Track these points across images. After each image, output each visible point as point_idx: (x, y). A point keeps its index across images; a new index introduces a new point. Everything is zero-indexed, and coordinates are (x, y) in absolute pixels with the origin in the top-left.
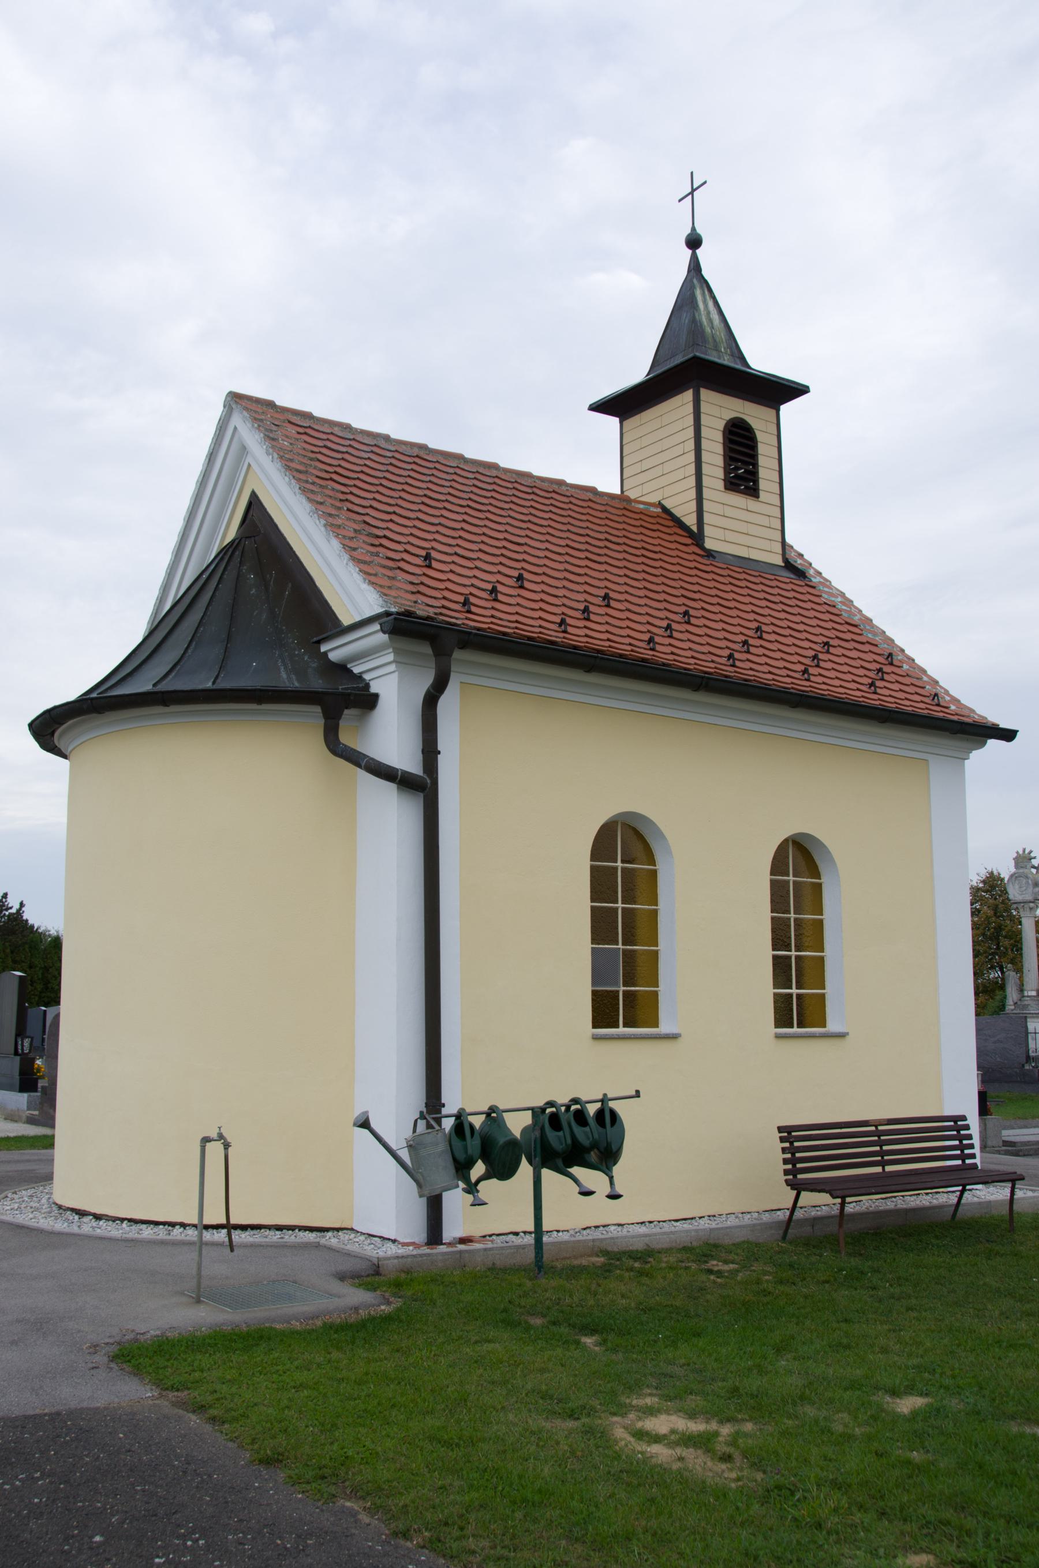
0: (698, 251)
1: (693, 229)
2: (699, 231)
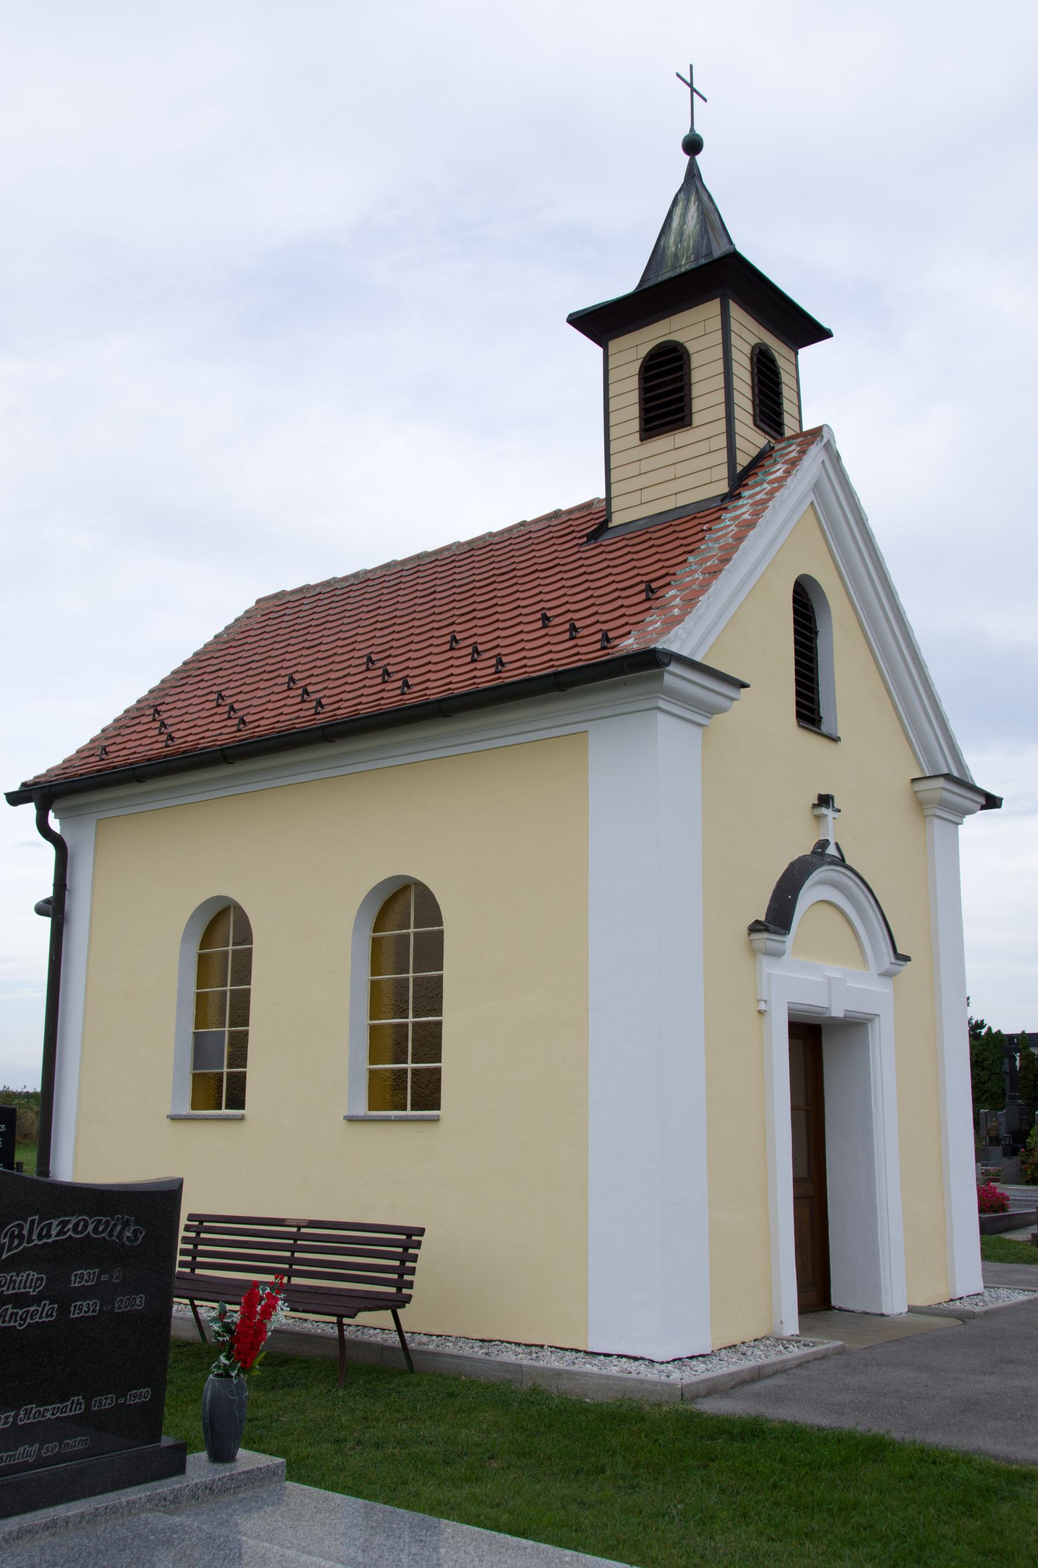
0: (697, 157)
1: (692, 129)
2: (698, 130)
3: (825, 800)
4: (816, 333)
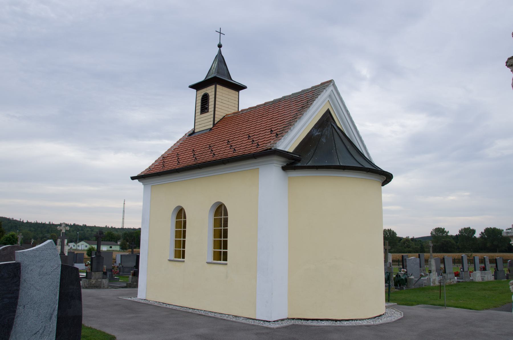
2: (221, 43)
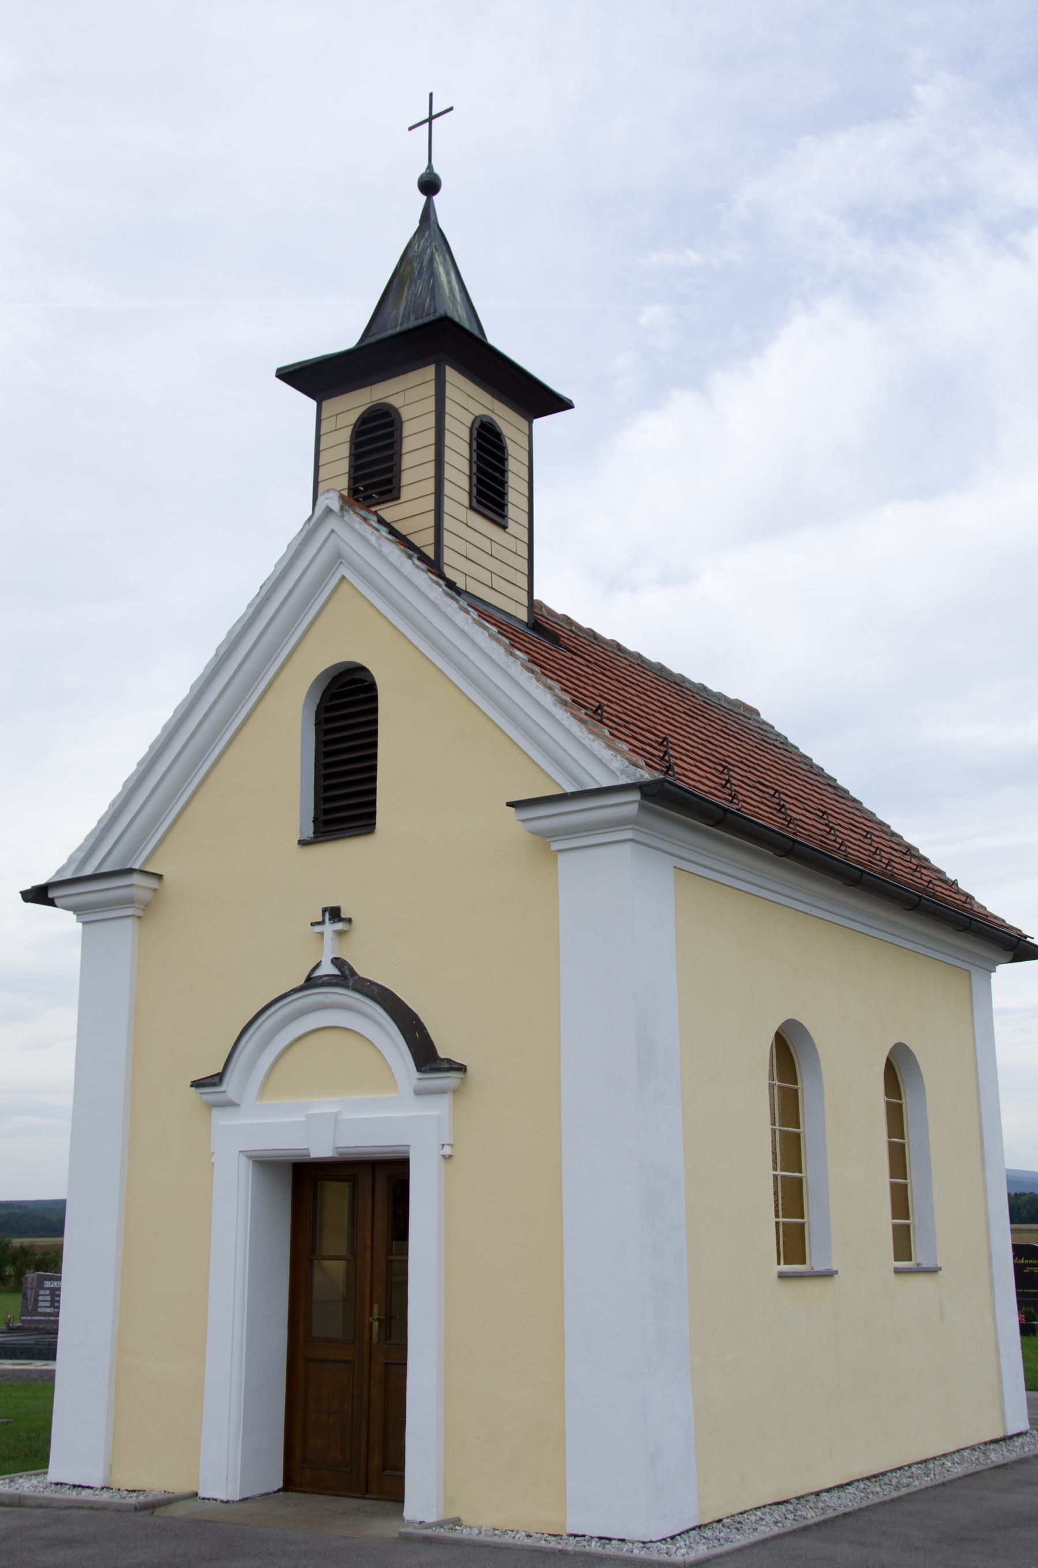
0: (435, 198)
1: (430, 166)
2: (437, 170)
3: (334, 914)
4: (552, 403)
